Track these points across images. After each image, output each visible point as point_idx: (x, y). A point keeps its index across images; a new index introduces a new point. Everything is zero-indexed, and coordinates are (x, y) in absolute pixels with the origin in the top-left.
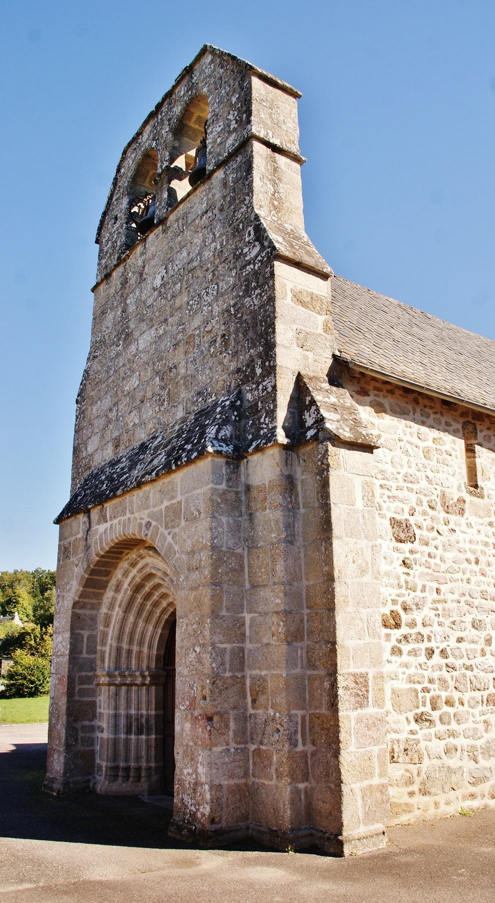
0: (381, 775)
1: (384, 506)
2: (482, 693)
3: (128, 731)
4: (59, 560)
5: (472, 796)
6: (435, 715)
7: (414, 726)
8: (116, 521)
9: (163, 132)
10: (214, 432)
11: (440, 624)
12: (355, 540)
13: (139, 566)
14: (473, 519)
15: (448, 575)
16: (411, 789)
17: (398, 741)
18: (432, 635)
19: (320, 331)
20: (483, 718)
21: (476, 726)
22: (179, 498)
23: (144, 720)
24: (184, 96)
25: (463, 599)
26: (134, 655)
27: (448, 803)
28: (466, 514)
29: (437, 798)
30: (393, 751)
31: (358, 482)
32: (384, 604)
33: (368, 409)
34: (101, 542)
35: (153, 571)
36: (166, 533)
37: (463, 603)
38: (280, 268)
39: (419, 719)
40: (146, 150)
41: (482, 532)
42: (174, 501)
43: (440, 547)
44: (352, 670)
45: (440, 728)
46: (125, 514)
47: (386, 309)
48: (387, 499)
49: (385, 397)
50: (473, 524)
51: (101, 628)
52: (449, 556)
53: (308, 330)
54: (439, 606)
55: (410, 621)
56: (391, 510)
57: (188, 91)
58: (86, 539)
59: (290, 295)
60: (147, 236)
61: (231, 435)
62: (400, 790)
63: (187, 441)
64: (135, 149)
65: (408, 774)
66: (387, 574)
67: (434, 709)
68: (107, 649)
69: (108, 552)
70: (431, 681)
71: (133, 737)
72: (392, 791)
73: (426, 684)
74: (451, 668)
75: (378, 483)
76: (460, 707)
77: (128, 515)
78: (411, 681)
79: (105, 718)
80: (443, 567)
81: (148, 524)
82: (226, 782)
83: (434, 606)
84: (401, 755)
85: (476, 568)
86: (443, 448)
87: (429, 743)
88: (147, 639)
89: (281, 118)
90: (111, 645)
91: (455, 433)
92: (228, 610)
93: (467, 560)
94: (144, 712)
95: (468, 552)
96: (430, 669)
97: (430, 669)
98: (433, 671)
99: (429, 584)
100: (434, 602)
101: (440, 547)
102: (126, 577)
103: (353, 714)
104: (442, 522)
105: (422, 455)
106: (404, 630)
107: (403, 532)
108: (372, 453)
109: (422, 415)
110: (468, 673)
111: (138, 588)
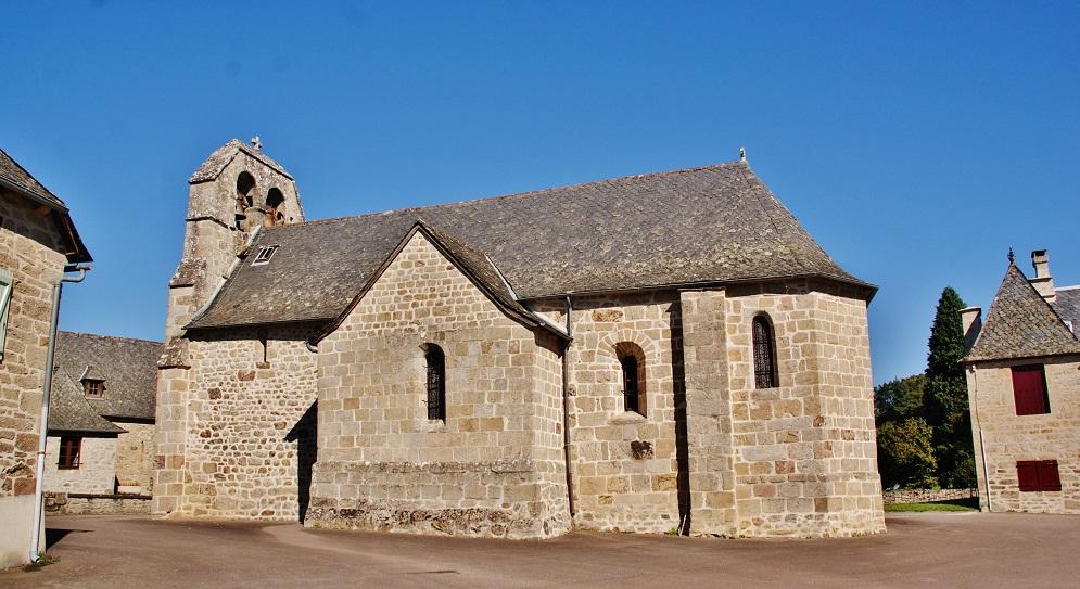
5: (241, 513)
6: (226, 475)
45: (228, 481)
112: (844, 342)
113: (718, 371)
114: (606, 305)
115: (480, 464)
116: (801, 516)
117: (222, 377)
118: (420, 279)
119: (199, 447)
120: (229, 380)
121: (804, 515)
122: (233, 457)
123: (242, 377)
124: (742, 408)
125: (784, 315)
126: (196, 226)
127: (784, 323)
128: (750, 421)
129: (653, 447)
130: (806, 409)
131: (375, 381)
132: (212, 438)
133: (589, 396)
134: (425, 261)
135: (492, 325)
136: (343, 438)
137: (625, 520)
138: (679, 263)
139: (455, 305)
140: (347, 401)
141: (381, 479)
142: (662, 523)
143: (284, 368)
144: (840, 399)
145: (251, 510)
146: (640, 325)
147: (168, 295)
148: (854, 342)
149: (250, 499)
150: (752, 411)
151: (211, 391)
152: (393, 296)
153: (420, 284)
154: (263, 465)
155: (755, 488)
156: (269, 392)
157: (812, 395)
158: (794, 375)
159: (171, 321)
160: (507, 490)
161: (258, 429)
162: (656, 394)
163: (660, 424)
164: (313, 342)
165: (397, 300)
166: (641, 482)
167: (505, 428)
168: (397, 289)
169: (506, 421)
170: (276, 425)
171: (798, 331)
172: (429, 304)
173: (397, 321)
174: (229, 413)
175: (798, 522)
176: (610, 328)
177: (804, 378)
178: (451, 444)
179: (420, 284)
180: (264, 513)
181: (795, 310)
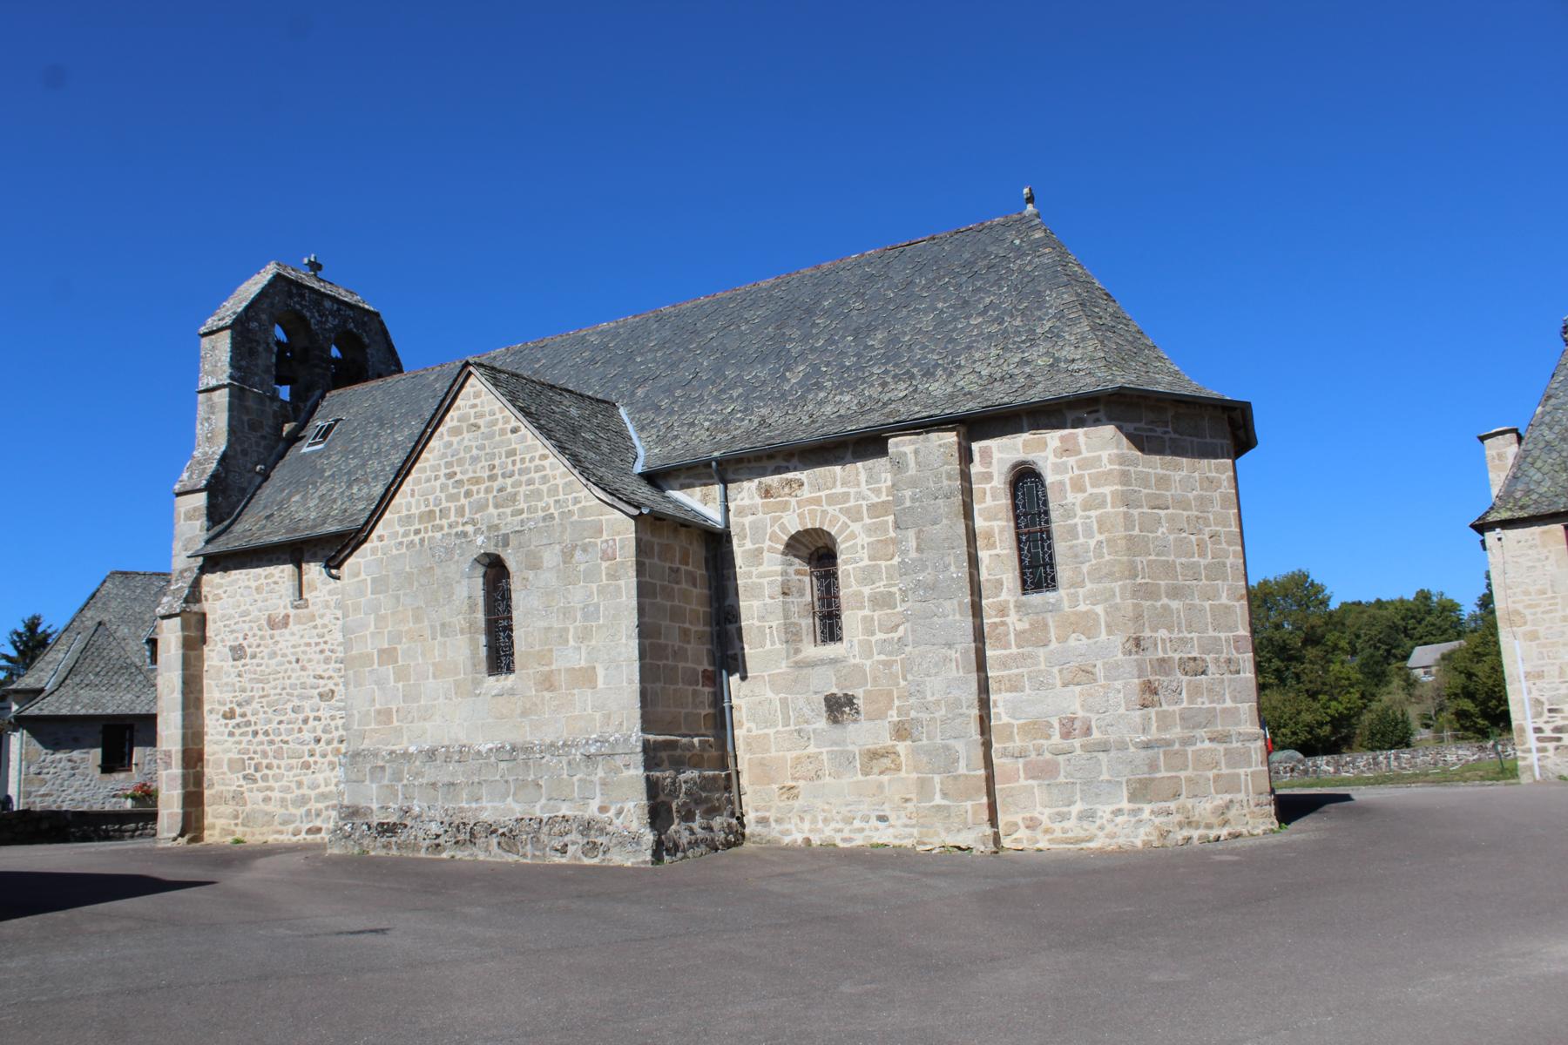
5: (281, 832)
6: (258, 775)
45: (261, 784)
67: (256, 770)
74: (272, 742)
106: (238, 720)
112: (1183, 504)
113: (953, 568)
114: (778, 471)
115: (565, 745)
116: (1104, 811)
117: (246, 626)
118: (475, 452)
119: (222, 734)
120: (256, 630)
121: (1109, 809)
122: (265, 747)
123: (272, 624)
124: (1001, 629)
125: (1065, 464)
126: (210, 399)
127: (1066, 478)
128: (1014, 650)
129: (859, 702)
130: (1108, 626)
131: (417, 619)
132: (238, 720)
133: (756, 623)
134: (481, 422)
135: (575, 518)
136: (379, 712)
137: (820, 825)
138: (901, 390)
139: (523, 489)
140: (381, 652)
141: (431, 773)
142: (877, 829)
143: (327, 607)
144: (1175, 604)
145: (291, 828)
146: (832, 499)
147: (172, 504)
148: (1203, 502)
149: (292, 810)
150: (1018, 634)
151: (232, 649)
152: (438, 483)
153: (475, 460)
154: (306, 758)
155: (1025, 765)
156: (308, 645)
157: (1118, 600)
158: (1085, 568)
159: (177, 546)
160: (604, 784)
161: (296, 702)
162: (861, 613)
163: (868, 663)
164: (333, 564)
165: (443, 488)
166: (844, 760)
167: (600, 684)
168: (444, 471)
169: (600, 672)
170: (321, 695)
171: (1090, 490)
172: (488, 490)
173: (445, 522)
174: (261, 681)
175: (1099, 822)
176: (785, 507)
177: (1105, 571)
178: (524, 714)
179: (475, 460)
180: (309, 831)
181: (1085, 454)
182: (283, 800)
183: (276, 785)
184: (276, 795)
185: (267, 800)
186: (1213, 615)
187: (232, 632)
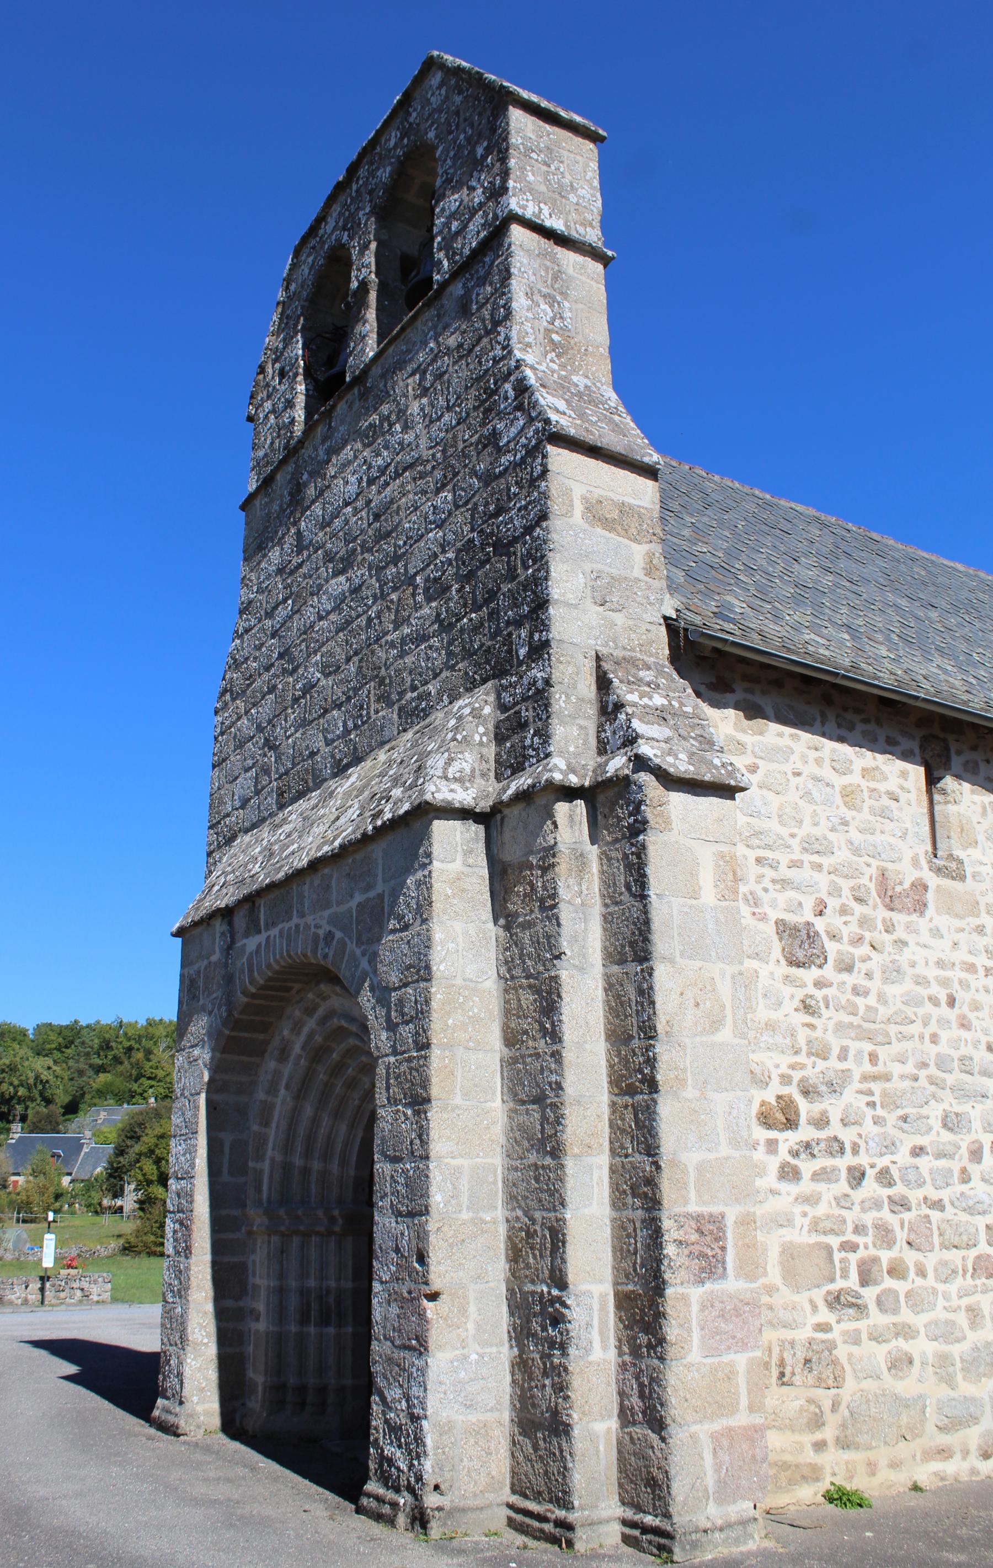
0: (751, 1409)
1: (766, 898)
2: (963, 1252)
3: (304, 1319)
4: (180, 1003)
5: (944, 1453)
6: (869, 1294)
7: (825, 1315)
8: (274, 932)
9: (361, 213)
10: (441, 763)
11: (877, 1121)
12: (699, 964)
13: (320, 1012)
14: (943, 921)
15: (893, 1029)
16: (818, 1436)
17: (792, 1343)
18: (861, 1142)
19: (638, 572)
20: (965, 1301)
21: (951, 1316)
22: (380, 888)
23: (331, 1299)
24: (396, 145)
25: (923, 1074)
26: (313, 1178)
27: (894, 1465)
28: (931, 911)
29: (871, 1455)
30: (782, 1364)
31: (706, 857)
32: (764, 1083)
33: (731, 712)
34: (251, 971)
35: (343, 1023)
36: (358, 952)
37: (923, 1082)
38: (558, 458)
39: (836, 1301)
40: (332, 248)
41: (964, 946)
42: (372, 894)
43: (877, 975)
44: (693, 1208)
45: (877, 1318)
46: (290, 918)
47: (786, 526)
48: (770, 886)
49: (764, 693)
50: (944, 931)
51: (255, 1128)
52: (894, 991)
53: (614, 572)
54: (876, 1087)
55: (817, 1116)
56: (778, 906)
57: (402, 139)
58: (226, 965)
59: (578, 508)
60: (333, 407)
61: (473, 771)
62: (797, 1437)
63: (396, 781)
64: (314, 248)
65: (813, 1408)
66: (771, 1026)
67: (864, 1282)
68: (266, 1166)
69: (263, 988)
70: (859, 1229)
71: (312, 1330)
72: (775, 1440)
73: (850, 1237)
74: (900, 1204)
75: (752, 855)
76: (919, 1281)
77: (295, 920)
78: (815, 1226)
79: (263, 1293)
80: (883, 1012)
81: (329, 936)
82: (461, 1418)
83: (864, 1086)
84: (797, 1370)
85: (951, 1014)
86: (882, 787)
87: (854, 1349)
88: (339, 1147)
89: (566, 181)
90: (273, 1159)
91: (906, 756)
92: (465, 1095)
93: (930, 999)
94: (332, 1284)
95: (933, 983)
96: (857, 1208)
97: (857, 1208)
98: (863, 1210)
99: (854, 1046)
100: (865, 1078)
101: (877, 975)
102: (299, 1033)
103: (696, 1293)
104: (880, 926)
105: (839, 800)
106: (805, 1132)
107: (801, 946)
108: (734, 799)
109: (839, 726)
110: (935, 1215)
111: (317, 1054)
120: (847, 897)
132: (805, 1132)
156: (971, 968)
161: (949, 1103)
182: (944, 1360)
183: (919, 1321)
184: (922, 1347)
185: (900, 1363)
186: (932, 1244)
187: (784, 883)
